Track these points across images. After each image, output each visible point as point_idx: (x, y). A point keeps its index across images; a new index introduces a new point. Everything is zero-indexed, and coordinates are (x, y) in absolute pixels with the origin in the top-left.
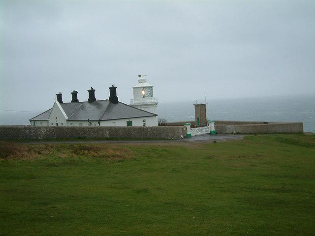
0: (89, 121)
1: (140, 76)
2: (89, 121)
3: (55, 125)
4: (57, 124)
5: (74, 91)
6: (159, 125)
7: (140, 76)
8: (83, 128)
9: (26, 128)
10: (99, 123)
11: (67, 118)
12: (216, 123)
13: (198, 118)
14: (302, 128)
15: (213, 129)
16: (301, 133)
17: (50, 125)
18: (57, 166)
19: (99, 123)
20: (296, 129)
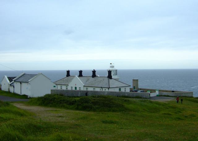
0: (101, 87)
1: (111, 64)
2: (101, 87)
3: (74, 89)
4: (76, 88)
5: (94, 70)
6: (130, 91)
7: (111, 64)
8: (97, 92)
9: (99, 92)
10: (109, 89)
11: (84, 85)
12: (159, 91)
13: (134, 87)
14: (193, 94)
15: (158, 94)
16: (192, 97)
17: (69, 88)
18: (177, 118)
19: (109, 89)
20: (190, 95)
